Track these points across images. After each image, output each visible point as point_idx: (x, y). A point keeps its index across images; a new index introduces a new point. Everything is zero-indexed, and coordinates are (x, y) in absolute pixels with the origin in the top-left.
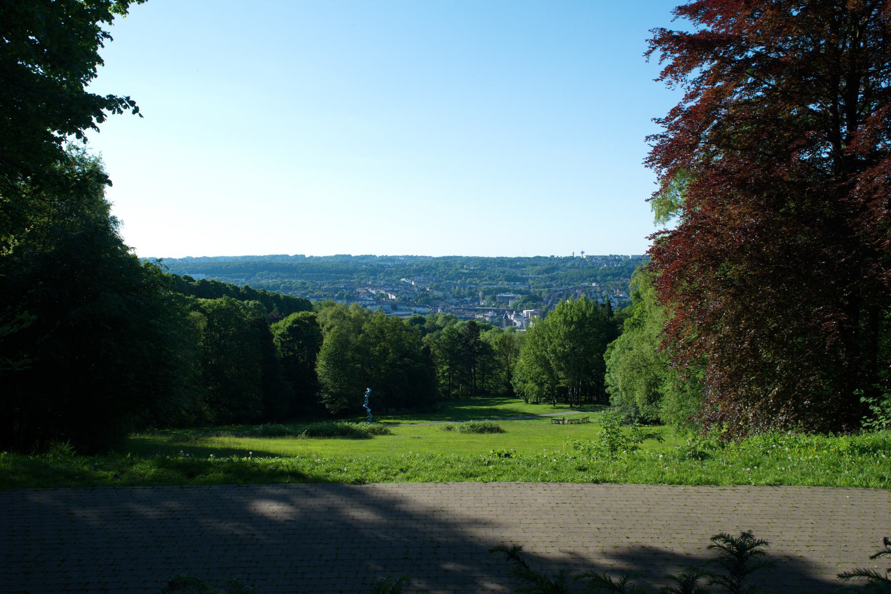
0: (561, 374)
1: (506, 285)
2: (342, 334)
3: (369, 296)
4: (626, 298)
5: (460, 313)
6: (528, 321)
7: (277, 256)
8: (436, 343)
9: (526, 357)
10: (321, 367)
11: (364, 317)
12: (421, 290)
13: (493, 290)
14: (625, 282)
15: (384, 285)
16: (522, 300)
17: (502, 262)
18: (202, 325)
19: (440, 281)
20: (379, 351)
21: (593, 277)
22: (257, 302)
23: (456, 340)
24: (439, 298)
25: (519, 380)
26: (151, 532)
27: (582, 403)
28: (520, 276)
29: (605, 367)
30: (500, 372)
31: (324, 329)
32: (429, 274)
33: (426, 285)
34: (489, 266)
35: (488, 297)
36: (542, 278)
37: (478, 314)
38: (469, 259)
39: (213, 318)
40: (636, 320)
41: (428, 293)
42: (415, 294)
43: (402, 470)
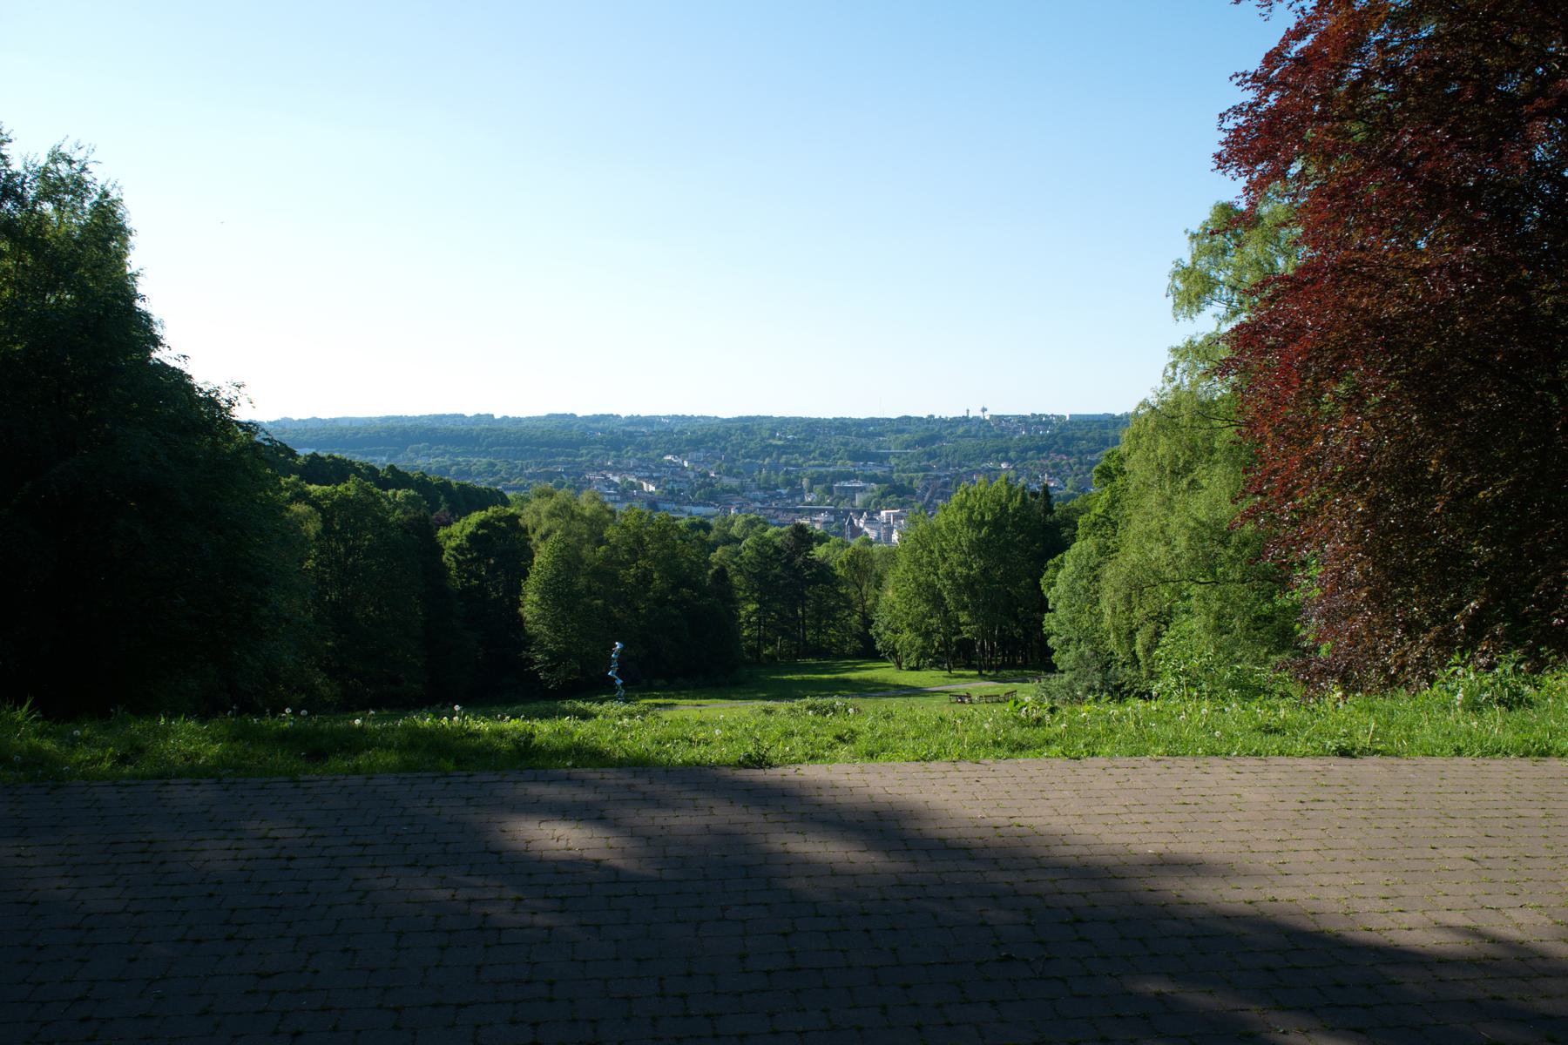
0: (964, 617)
1: (849, 466)
2: (567, 545)
3: (609, 487)
4: (1061, 489)
5: (769, 516)
6: (890, 530)
7: (444, 416)
8: (735, 563)
9: (899, 585)
10: (530, 605)
11: (607, 516)
12: (701, 476)
13: (827, 476)
14: (1058, 461)
15: (635, 467)
16: (879, 493)
17: (842, 426)
18: (313, 527)
19: (735, 460)
20: (634, 576)
21: (1002, 453)
22: (412, 492)
23: (770, 557)
24: (732, 491)
25: (887, 628)
26: (211, 895)
27: (998, 668)
28: (873, 449)
29: (1046, 601)
30: (849, 615)
31: (535, 538)
32: (714, 448)
33: (710, 466)
34: (819, 434)
35: (818, 488)
36: (912, 456)
37: (801, 518)
38: (784, 422)
39: (332, 518)
40: (1100, 516)
41: (714, 481)
42: (689, 482)
43: (840, 738)
